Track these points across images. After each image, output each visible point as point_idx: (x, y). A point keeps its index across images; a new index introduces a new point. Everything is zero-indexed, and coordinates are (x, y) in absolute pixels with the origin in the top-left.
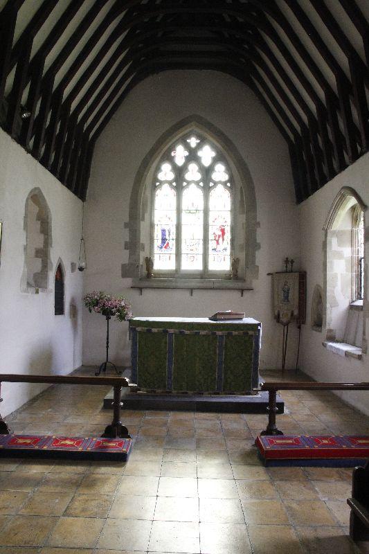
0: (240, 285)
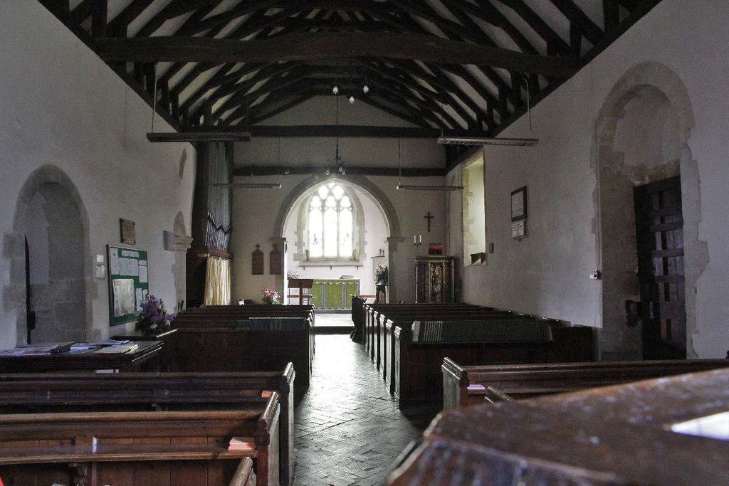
0: (356, 264)
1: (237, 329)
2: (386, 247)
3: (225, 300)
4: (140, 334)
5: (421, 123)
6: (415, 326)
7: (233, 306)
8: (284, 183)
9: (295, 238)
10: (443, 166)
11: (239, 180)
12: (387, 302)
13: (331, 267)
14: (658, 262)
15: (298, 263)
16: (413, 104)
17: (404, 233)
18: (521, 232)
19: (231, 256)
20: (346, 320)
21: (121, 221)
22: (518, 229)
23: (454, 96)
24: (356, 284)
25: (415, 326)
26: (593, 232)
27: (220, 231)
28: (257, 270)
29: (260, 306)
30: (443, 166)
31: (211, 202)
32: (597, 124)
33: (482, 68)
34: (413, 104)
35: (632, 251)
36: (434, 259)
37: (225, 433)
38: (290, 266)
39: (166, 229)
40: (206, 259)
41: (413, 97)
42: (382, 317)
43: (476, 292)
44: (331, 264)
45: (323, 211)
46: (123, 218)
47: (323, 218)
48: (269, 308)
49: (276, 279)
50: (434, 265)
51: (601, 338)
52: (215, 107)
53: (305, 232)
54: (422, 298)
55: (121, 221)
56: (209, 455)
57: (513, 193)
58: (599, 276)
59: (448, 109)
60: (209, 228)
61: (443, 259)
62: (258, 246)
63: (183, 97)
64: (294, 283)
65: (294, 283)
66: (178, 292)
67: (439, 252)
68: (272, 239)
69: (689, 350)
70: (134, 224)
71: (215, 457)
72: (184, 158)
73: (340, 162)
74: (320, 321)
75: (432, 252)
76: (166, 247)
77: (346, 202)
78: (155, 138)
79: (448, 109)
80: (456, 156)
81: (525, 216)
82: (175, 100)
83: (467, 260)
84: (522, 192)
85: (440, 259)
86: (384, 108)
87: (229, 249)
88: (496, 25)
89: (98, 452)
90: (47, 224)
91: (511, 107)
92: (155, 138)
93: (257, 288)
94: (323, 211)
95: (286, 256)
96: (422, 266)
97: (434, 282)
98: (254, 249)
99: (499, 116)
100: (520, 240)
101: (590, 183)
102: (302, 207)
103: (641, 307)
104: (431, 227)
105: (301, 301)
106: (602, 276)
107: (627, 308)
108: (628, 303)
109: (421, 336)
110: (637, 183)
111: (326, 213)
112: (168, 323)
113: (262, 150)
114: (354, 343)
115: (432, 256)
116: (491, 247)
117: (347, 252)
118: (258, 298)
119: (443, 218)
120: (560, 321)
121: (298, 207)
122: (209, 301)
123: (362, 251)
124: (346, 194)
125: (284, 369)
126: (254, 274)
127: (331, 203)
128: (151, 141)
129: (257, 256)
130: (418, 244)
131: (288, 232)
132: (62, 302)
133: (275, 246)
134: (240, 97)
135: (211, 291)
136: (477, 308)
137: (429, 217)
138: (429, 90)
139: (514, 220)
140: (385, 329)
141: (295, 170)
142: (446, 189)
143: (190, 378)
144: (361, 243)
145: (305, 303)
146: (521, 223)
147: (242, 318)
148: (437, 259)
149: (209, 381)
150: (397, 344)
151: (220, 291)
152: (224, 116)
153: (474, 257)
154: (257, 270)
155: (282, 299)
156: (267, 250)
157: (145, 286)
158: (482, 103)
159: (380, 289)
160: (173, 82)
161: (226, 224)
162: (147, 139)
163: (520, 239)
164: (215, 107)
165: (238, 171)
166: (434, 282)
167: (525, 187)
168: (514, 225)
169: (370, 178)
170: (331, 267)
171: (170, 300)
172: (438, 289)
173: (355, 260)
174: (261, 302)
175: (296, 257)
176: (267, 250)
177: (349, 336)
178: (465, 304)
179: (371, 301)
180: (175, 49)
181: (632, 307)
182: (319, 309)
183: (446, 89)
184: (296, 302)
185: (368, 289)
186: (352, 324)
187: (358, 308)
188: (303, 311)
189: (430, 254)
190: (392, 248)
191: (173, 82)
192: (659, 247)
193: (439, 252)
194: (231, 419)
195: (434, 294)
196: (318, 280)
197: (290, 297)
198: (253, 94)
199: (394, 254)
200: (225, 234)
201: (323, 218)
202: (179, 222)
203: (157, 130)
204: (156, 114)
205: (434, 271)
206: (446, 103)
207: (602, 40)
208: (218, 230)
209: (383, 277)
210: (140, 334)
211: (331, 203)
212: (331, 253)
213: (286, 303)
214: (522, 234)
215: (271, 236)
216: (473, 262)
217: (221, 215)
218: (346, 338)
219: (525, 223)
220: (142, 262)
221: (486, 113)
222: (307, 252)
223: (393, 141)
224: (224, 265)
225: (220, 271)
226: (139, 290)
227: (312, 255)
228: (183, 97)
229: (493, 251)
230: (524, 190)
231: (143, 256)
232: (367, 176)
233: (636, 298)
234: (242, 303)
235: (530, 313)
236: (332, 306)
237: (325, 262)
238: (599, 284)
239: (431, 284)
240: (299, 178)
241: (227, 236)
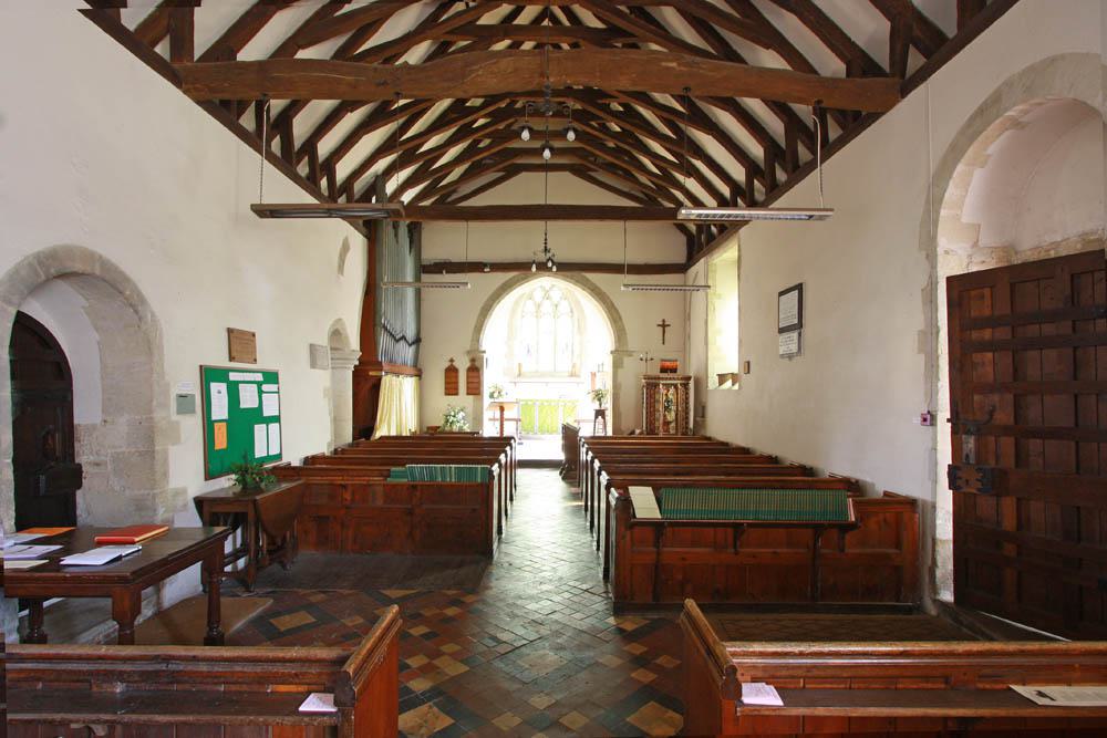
5: (652, 206)
10: (681, 258)
11: (426, 278)
16: (644, 179)
17: (633, 343)
18: (794, 348)
21: (230, 331)
22: (789, 343)
26: (920, 351)
27: (402, 342)
30: (681, 258)
34: (644, 179)
36: (666, 379)
40: (379, 379)
43: (724, 425)
46: (231, 327)
50: (667, 386)
52: (391, 187)
54: (651, 431)
55: (230, 331)
57: (781, 294)
61: (678, 379)
62: (452, 361)
63: (343, 169)
67: (674, 370)
68: (468, 352)
70: (254, 335)
72: (345, 248)
73: (549, 255)
75: (663, 370)
76: (313, 365)
77: (564, 306)
78: (266, 212)
80: (700, 242)
81: (800, 325)
83: (713, 382)
84: (797, 291)
85: (674, 379)
87: (415, 365)
88: (767, 47)
90: (96, 336)
91: (781, 176)
92: (266, 212)
97: (667, 408)
98: (447, 364)
99: (764, 190)
113: (445, 240)
116: (748, 367)
119: (681, 325)
120: (857, 481)
126: (447, 394)
128: (261, 217)
129: (451, 372)
132: (119, 450)
133: (473, 360)
136: (724, 447)
137: (664, 326)
138: (666, 159)
142: (687, 290)
151: (400, 411)
152: (407, 197)
153: (722, 378)
154: (451, 389)
156: (463, 365)
158: (756, 150)
160: (325, 147)
161: (410, 334)
163: (790, 356)
164: (391, 187)
165: (424, 269)
166: (667, 408)
167: (801, 284)
169: (592, 276)
170: (547, 383)
172: (671, 416)
176: (463, 365)
178: (709, 439)
186: (561, 456)
189: (661, 372)
191: (325, 147)
193: (674, 370)
195: (667, 423)
196: (923, 75)
204: (265, 161)
205: (666, 394)
207: (939, 49)
208: (397, 341)
214: (795, 351)
215: (468, 348)
216: (720, 384)
219: (800, 334)
221: (744, 186)
223: (616, 226)
228: (343, 169)
230: (799, 287)
232: (636, 626)
235: (808, 462)
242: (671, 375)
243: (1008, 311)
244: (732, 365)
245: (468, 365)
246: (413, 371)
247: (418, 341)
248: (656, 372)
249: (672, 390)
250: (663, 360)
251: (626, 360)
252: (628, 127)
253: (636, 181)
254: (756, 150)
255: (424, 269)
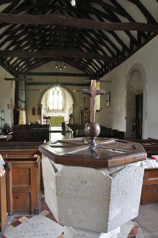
0: (63, 111)
1: (30, 132)
2: (72, 107)
3: (25, 123)
4: (3, 133)
6: (77, 131)
7: (27, 125)
8: (41, 88)
9: (45, 103)
12: (72, 124)
13: (56, 112)
14: (140, 115)
15: (45, 111)
17: (77, 103)
19: (26, 109)
20: (60, 128)
23: (88, 68)
24: (63, 118)
25: (77, 131)
27: (23, 103)
28: (34, 114)
29: (34, 124)
31: (20, 94)
32: (127, 77)
33: (88, 73)
35: (134, 112)
36: (85, 111)
37: (33, 153)
38: (43, 112)
39: (8, 103)
41: (81, 63)
42: (69, 128)
44: (56, 111)
45: (53, 95)
47: (53, 97)
48: (38, 125)
49: (39, 116)
51: (125, 135)
52: (20, 65)
53: (48, 102)
56: (30, 157)
57: (107, 94)
58: (126, 118)
59: (90, 67)
60: (20, 102)
61: (88, 111)
62: (34, 107)
63: (11, 63)
64: (45, 118)
65: (45, 118)
66: (12, 121)
67: (87, 109)
68: (38, 105)
69: (142, 138)
71: (31, 158)
73: (58, 83)
74: (52, 129)
75: (85, 109)
78: (6, 79)
79: (90, 67)
81: (110, 100)
82: (9, 64)
86: (72, 65)
88: (103, 46)
89: (7, 157)
92: (6, 79)
93: (34, 119)
94: (53, 95)
95: (42, 110)
96: (82, 113)
97: (86, 118)
100: (108, 107)
101: (125, 94)
102: (47, 94)
103: (136, 126)
104: (85, 101)
105: (47, 123)
106: (126, 118)
107: (133, 127)
108: (133, 125)
109: (78, 134)
110: (137, 94)
111: (54, 95)
112: (11, 130)
114: (62, 136)
115: (85, 110)
116: (101, 109)
117: (61, 108)
118: (34, 122)
121: (45, 96)
122: (20, 123)
123: (65, 107)
124: (60, 90)
125: (44, 141)
127: (56, 92)
129: (34, 110)
130: (81, 107)
131: (43, 103)
133: (39, 107)
134: (28, 63)
135: (20, 120)
139: (107, 101)
140: (70, 131)
141: (45, 84)
143: (22, 143)
144: (65, 105)
145: (48, 124)
146: (109, 102)
147: (31, 128)
148: (86, 111)
149: (27, 144)
150: (72, 135)
151: (23, 120)
153: (97, 111)
154: (34, 114)
155: (41, 122)
157: (4, 120)
158: (100, 66)
159: (70, 119)
161: (24, 100)
162: (4, 80)
164: (20, 65)
165: (27, 84)
166: (86, 118)
168: (107, 103)
169: (68, 87)
171: (10, 122)
173: (63, 110)
174: (35, 123)
175: (45, 109)
176: (36, 108)
177: (61, 133)
179: (67, 123)
180: (12, 54)
181: (134, 127)
182: (52, 125)
183: (90, 61)
184: (45, 123)
185: (67, 119)
186: (62, 130)
187: (63, 125)
188: (47, 126)
190: (74, 108)
192: (140, 112)
193: (87, 109)
194: (34, 151)
197: (43, 122)
198: (31, 61)
199: (75, 109)
200: (24, 103)
201: (53, 97)
202: (11, 101)
203: (7, 77)
204: (6, 71)
206: (90, 65)
208: (22, 102)
209: (71, 116)
210: (3, 133)
211: (56, 92)
212: (56, 108)
213: (42, 124)
215: (38, 104)
217: (23, 97)
218: (60, 134)
219: (110, 103)
220: (2, 113)
222: (48, 108)
224: (24, 112)
225: (23, 115)
226: (2, 121)
227: (50, 109)
228: (11, 63)
229: (101, 110)
230: (110, 93)
231: (3, 111)
232: (67, 86)
233: (135, 124)
234: (29, 124)
235: (110, 128)
236: (56, 124)
237: (54, 111)
238: (126, 120)
239: (84, 118)
240: (46, 86)
241: (24, 104)
242: (87, 110)
243: (51, 130)
244: (99, 108)
245: (38, 108)
246: (25, 109)
247: (25, 102)
248: (83, 109)
249: (87, 114)
250: (85, 107)
251: (76, 107)
252: (78, 45)
253: (79, 65)
254: (100, 66)
255: (27, 84)
